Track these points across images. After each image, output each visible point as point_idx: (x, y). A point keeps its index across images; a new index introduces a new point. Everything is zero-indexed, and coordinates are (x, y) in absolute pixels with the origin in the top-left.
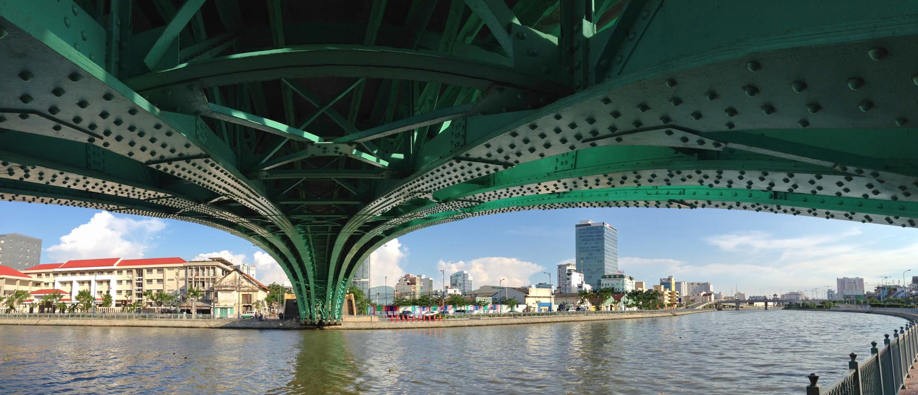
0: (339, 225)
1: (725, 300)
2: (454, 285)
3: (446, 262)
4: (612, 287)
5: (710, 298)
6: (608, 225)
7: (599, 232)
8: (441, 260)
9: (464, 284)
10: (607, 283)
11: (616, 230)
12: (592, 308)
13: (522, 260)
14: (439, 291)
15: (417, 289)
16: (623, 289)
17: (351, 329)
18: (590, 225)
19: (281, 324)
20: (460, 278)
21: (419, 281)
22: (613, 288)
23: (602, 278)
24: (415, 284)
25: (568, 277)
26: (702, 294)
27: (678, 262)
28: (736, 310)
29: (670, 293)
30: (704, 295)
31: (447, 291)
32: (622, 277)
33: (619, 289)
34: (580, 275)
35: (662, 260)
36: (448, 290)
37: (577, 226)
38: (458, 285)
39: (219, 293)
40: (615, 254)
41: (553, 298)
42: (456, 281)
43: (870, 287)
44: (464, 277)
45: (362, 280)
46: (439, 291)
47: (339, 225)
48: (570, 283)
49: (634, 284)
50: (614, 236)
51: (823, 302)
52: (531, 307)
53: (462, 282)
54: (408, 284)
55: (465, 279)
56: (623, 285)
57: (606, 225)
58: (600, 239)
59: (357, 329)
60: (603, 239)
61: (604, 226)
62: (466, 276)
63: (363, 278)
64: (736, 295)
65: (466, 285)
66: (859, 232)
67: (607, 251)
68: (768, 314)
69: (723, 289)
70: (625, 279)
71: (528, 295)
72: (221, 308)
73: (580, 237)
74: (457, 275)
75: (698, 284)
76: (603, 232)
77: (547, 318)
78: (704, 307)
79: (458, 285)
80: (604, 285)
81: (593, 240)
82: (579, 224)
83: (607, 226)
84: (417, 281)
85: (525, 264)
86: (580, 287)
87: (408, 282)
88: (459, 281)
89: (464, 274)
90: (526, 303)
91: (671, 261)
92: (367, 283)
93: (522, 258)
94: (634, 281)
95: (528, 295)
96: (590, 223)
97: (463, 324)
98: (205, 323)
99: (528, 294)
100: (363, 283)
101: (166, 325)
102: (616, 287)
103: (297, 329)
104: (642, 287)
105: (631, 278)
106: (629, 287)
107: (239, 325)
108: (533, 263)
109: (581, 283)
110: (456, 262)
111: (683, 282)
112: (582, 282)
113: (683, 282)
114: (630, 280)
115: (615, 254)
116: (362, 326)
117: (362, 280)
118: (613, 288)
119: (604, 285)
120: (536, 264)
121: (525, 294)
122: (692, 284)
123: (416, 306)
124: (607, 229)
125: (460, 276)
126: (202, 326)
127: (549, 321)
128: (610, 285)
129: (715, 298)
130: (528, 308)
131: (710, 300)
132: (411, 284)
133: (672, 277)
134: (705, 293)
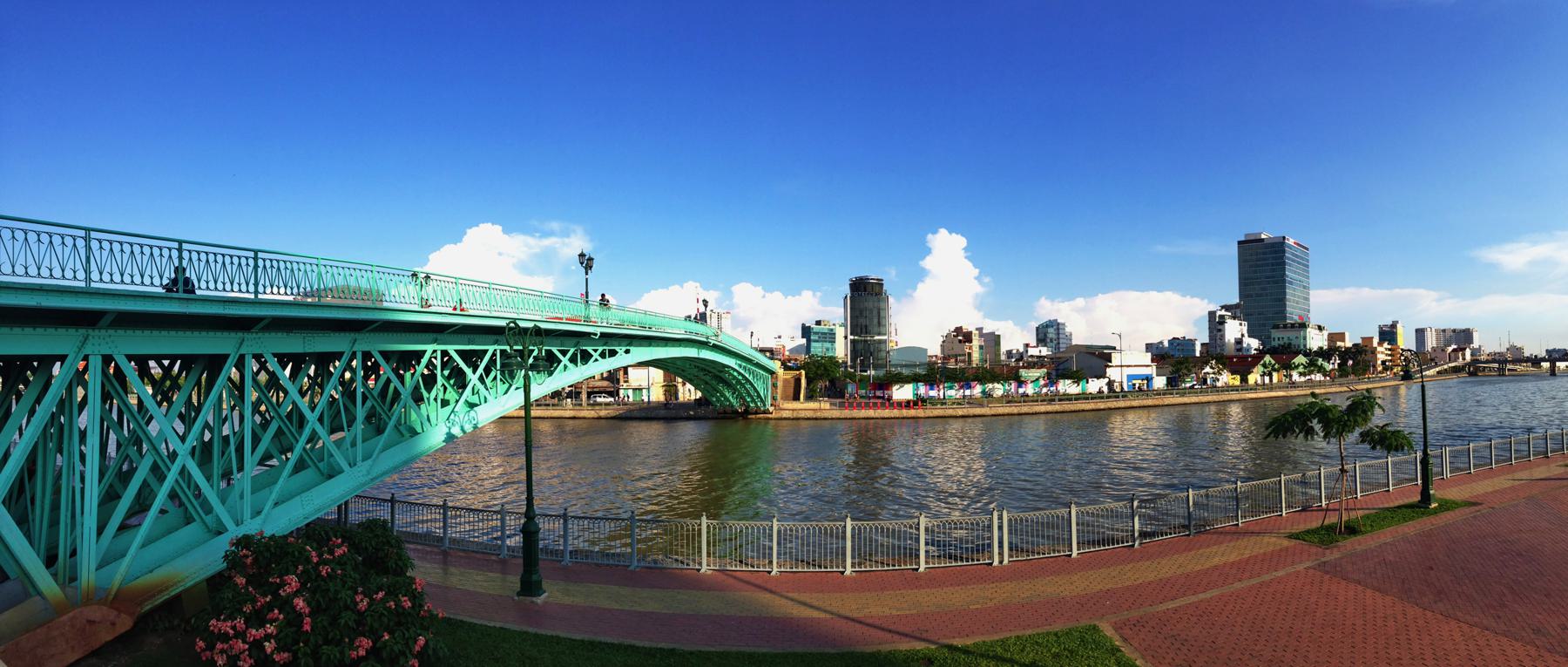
0: (113, 365)
1: (1490, 358)
2: (1042, 339)
3: (1053, 300)
4: (1287, 342)
5: (1464, 355)
6: (1291, 240)
7: (1276, 252)
8: (1043, 298)
9: (1058, 339)
10: (1280, 336)
11: (1307, 249)
12: (1236, 381)
13: (1184, 296)
14: (1014, 352)
15: (974, 349)
16: (1305, 346)
17: (785, 419)
18: (1263, 239)
19: (692, 413)
20: (1051, 330)
21: (977, 337)
22: (1290, 344)
23: (1273, 328)
24: (971, 342)
25: (1220, 327)
26: (1450, 349)
27: (1433, 294)
28: (1499, 375)
29: (1390, 350)
30: (1454, 350)
31: (1027, 351)
32: (1303, 326)
33: (1299, 346)
34: (1241, 324)
35: (1406, 291)
36: (1029, 349)
37: (1240, 243)
38: (1048, 340)
39: (630, 369)
40: (1304, 287)
41: (1155, 367)
42: (1045, 335)
43: (1527, 354)
44: (1058, 329)
45: (877, 338)
46: (1014, 352)
47: (113, 365)
48: (1223, 336)
49: (1326, 337)
50: (1302, 258)
51: (908, 402)
52: (1114, 381)
53: (1054, 336)
54: (960, 341)
55: (1061, 331)
56: (1305, 338)
57: (1288, 240)
58: (1278, 264)
59: (793, 419)
60: (1284, 263)
61: (1284, 243)
62: (1061, 327)
63: (879, 334)
64: (1508, 349)
65: (1061, 341)
66: (448, 371)
67: (1291, 283)
68: (1556, 382)
69: (1488, 342)
70: (1308, 330)
71: (1110, 364)
72: (634, 389)
73: (1245, 261)
74: (1047, 326)
75: (1454, 331)
76: (1284, 252)
77: (958, 410)
78: (1438, 372)
79: (1048, 340)
80: (1276, 339)
81: (1267, 265)
82: (1243, 239)
83: (1291, 241)
84: (973, 337)
85: (1188, 300)
86: (1239, 342)
87: (960, 338)
88: (1050, 336)
89: (1058, 324)
90: (1108, 375)
91: (1422, 291)
92: (885, 341)
93: (1185, 291)
94: (1325, 333)
95: (1110, 364)
96: (1263, 236)
97: (954, 414)
98: (593, 412)
99: (1111, 362)
100: (880, 342)
101: (542, 415)
102: (1293, 342)
103: (713, 418)
104: (1343, 340)
105: (1320, 328)
106: (1316, 341)
107: (638, 415)
108: (1203, 299)
109: (1240, 337)
110: (1072, 298)
111: (1429, 329)
112: (1243, 335)
113: (1429, 329)
114: (1317, 331)
115: (1304, 287)
116: (802, 414)
117: (877, 338)
118: (1290, 344)
119: (1276, 339)
120: (1206, 301)
121: (1104, 363)
122: (1444, 331)
123: (919, 384)
124: (1290, 247)
125: (1052, 327)
126: (589, 416)
127: (1102, 407)
128: (1285, 340)
129: (1472, 355)
130: (1110, 384)
131: (1464, 359)
132: (965, 342)
133: (1397, 322)
134: (1455, 347)
